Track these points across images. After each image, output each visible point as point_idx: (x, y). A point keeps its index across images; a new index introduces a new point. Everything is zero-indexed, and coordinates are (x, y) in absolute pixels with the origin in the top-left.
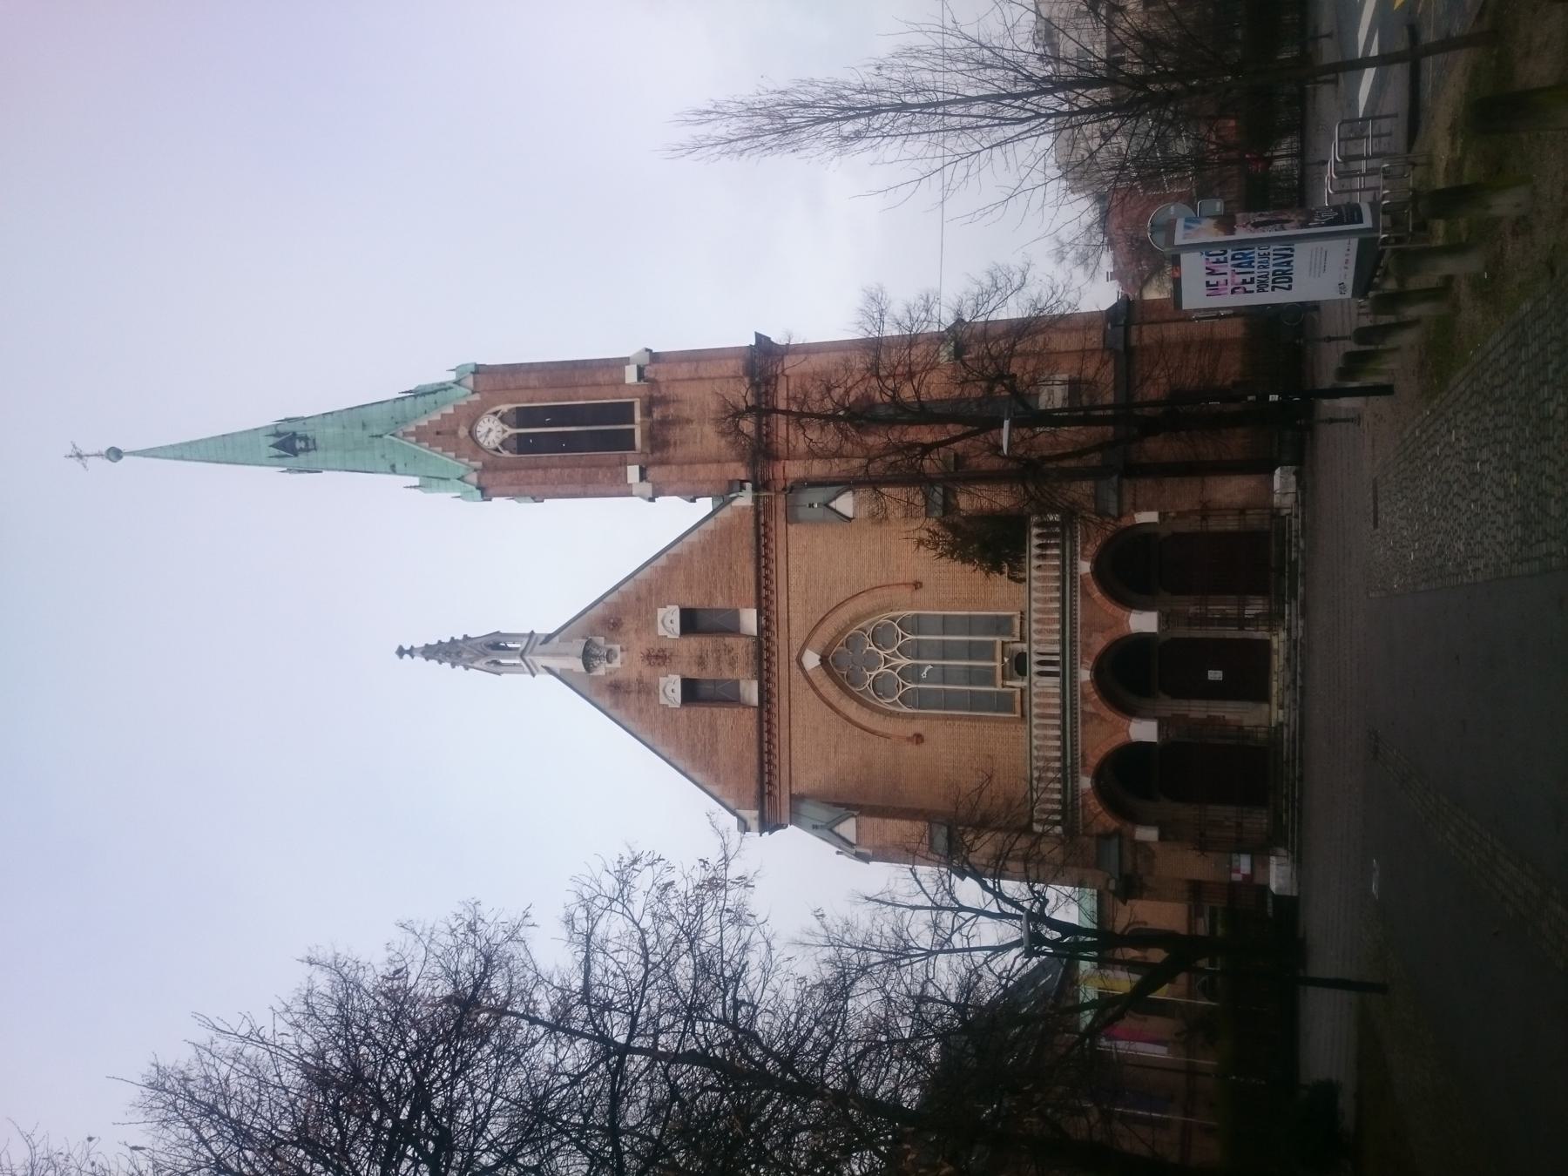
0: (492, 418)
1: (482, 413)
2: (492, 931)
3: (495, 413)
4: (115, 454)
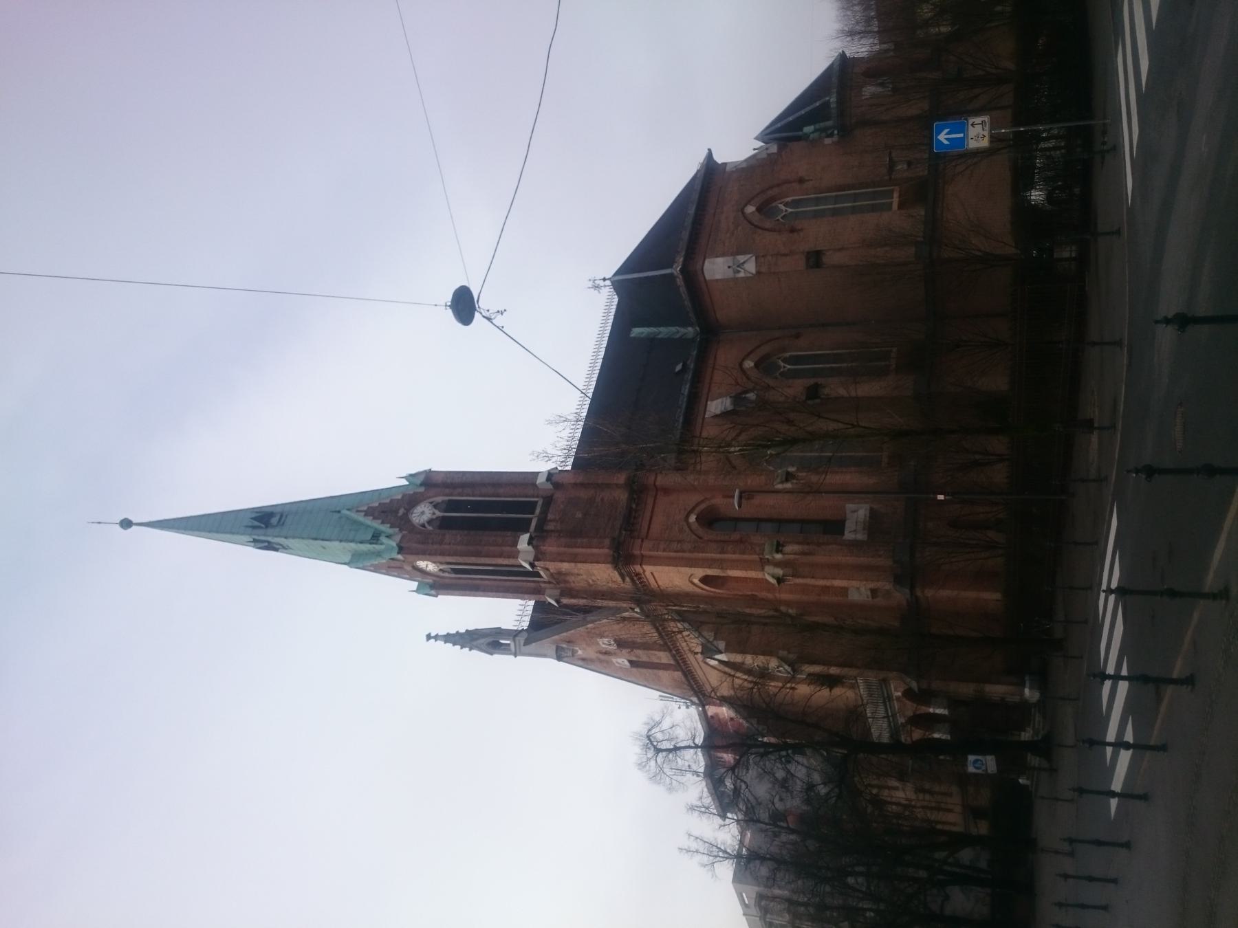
0: (427, 505)
3: (431, 503)
4: (126, 524)
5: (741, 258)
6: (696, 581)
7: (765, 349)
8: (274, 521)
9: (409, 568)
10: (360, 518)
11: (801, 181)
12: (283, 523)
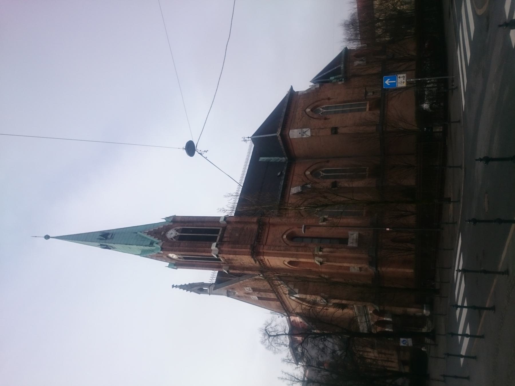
0: (174, 230)
1: (172, 228)
2: (287, 365)
3: (175, 229)
4: (47, 237)
5: (305, 130)
6: (286, 263)
7: (314, 167)
8: (109, 236)
9: (165, 257)
10: (145, 235)
11: (329, 99)
12: (113, 238)
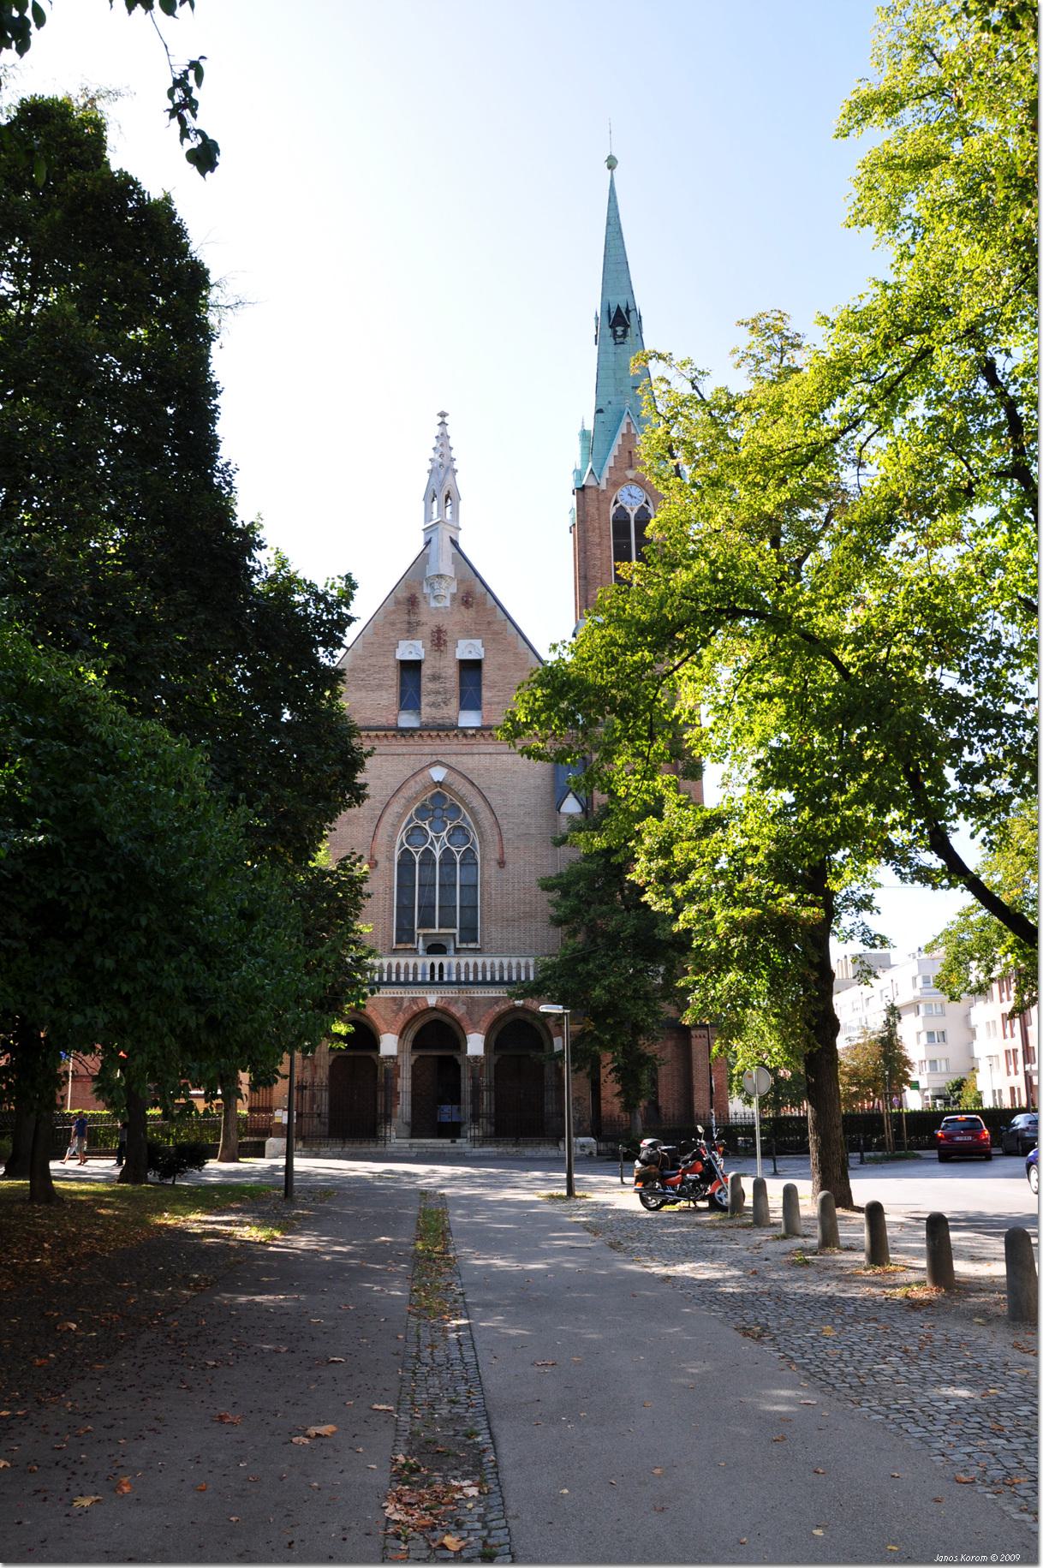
4: (612, 163)
